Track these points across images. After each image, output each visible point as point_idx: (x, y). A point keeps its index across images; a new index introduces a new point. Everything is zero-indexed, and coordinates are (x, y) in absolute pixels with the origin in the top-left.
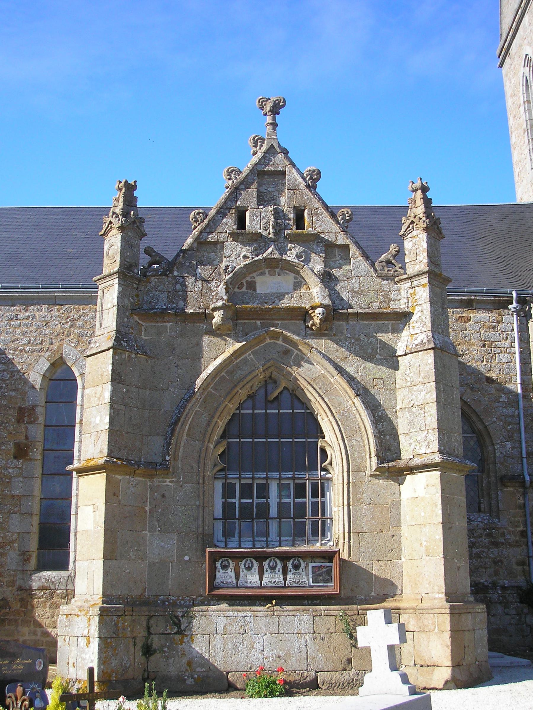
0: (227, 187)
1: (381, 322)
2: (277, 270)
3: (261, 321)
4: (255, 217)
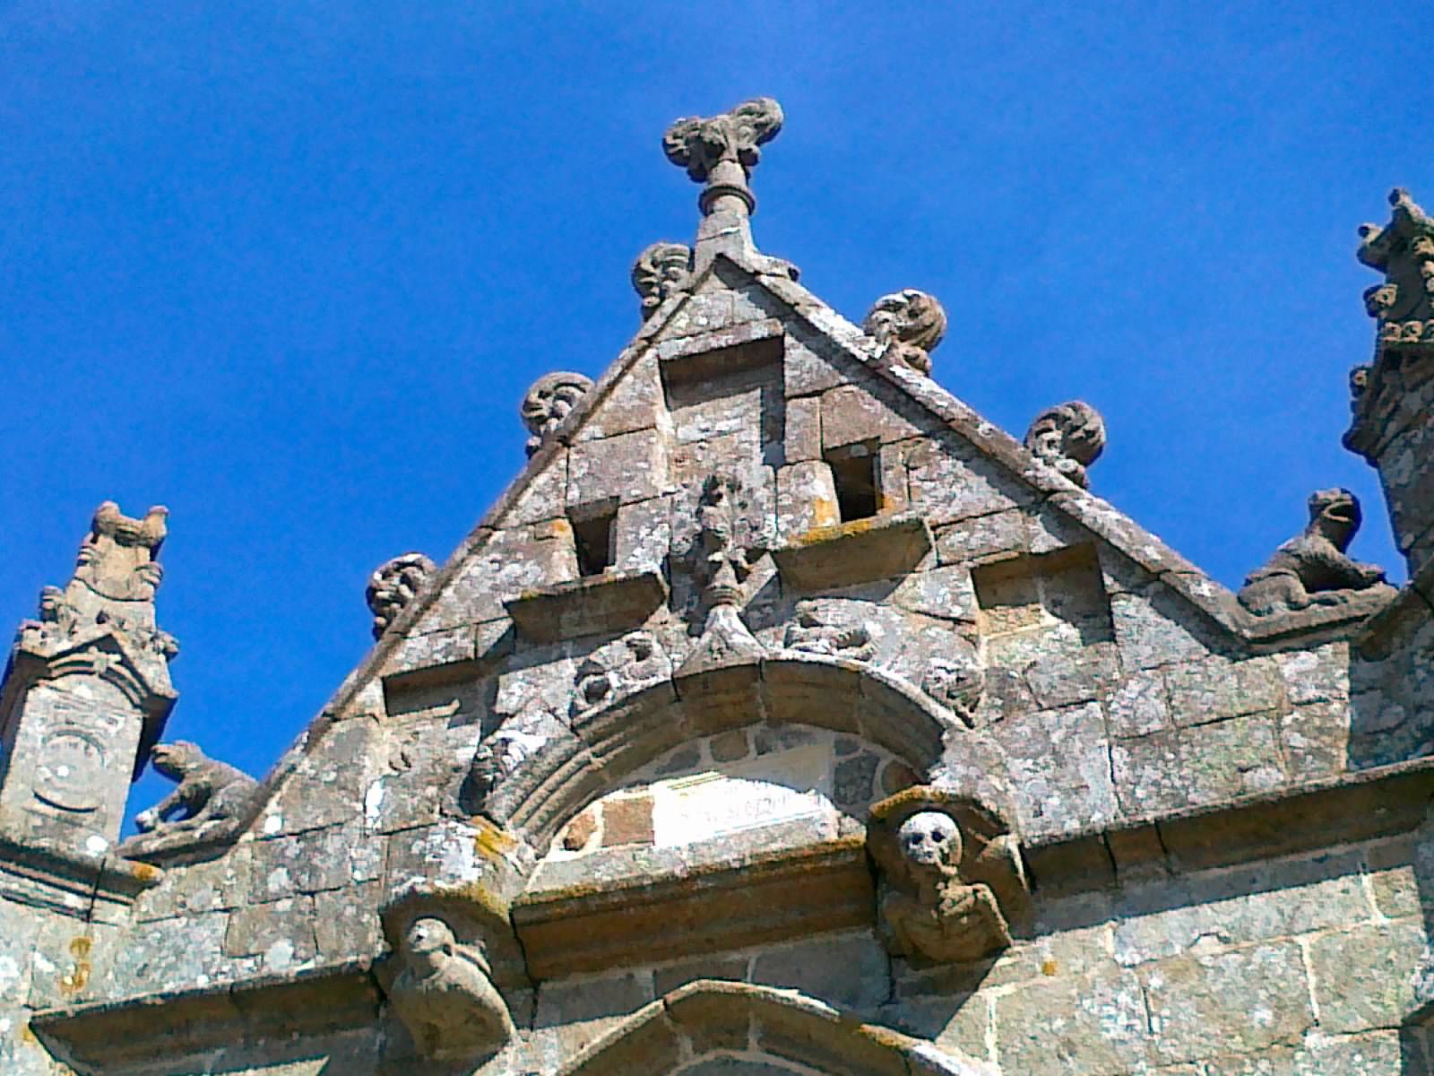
0: (537, 510)
1: (1309, 856)
2: (752, 732)
3: (659, 967)
4: (643, 532)
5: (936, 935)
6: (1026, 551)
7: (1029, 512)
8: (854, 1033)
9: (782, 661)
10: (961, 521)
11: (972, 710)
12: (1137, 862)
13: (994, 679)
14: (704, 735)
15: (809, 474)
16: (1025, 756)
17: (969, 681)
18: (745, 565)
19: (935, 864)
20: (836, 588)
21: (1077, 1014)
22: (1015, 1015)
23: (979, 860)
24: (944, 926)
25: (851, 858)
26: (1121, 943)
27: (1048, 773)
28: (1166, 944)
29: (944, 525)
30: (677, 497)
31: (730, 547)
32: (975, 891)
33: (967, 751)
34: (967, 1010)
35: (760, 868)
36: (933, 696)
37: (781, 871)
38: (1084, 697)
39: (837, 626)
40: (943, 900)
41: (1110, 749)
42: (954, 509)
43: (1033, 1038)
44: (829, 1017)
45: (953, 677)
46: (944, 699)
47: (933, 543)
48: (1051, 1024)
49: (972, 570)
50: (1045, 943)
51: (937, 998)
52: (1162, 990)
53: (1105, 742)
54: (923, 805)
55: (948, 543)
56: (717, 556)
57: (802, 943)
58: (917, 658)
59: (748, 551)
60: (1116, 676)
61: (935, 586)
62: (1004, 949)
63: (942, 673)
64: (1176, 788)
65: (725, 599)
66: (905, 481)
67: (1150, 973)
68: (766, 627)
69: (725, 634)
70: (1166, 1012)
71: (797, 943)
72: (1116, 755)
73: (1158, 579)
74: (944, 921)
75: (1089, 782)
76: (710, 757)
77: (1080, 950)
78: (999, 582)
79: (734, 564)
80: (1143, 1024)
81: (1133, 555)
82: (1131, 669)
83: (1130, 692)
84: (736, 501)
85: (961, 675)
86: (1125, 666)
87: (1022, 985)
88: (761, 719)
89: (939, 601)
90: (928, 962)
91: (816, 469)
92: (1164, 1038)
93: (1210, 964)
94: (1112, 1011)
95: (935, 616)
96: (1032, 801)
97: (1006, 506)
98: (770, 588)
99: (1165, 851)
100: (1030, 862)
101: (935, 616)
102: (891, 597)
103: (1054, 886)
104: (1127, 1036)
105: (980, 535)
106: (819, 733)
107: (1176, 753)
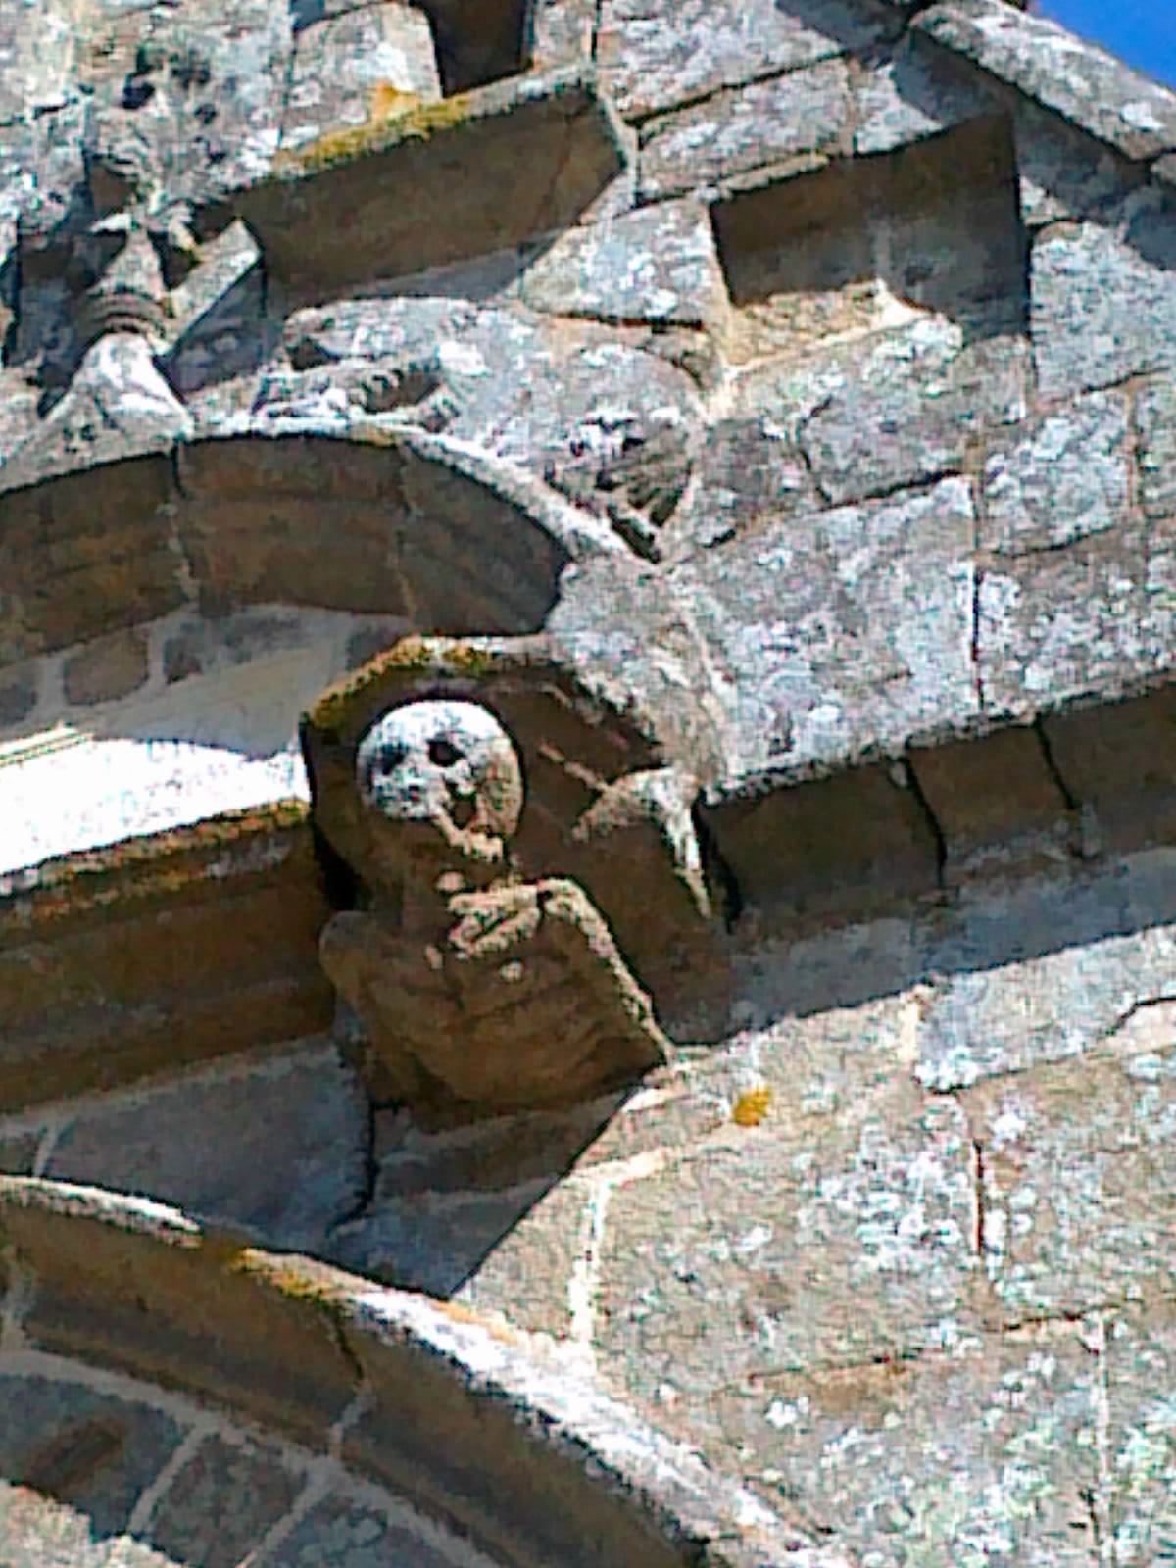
2: (162, 631)
5: (440, 1016)
6: (848, 149)
7: (865, 66)
8: (225, 1270)
9: (223, 439)
10: (706, 98)
11: (657, 520)
12: (1000, 836)
13: (724, 446)
14: (52, 648)
15: (370, 34)
16: (768, 616)
17: (652, 446)
18: (185, 240)
19: (428, 820)
20: (384, 273)
21: (802, 1215)
22: (652, 1227)
23: (580, 833)
24: (455, 988)
25: (276, 854)
26: (937, 1035)
27: (821, 650)
28: (1050, 1030)
29: (662, 111)
30: (62, 117)
31: (154, 205)
32: (543, 897)
33: (610, 599)
34: (538, 1222)
35: (59, 893)
36: (561, 489)
37: (107, 897)
38: (931, 467)
39: (372, 357)
40: (457, 919)
41: (978, 581)
42: (692, 74)
43: (688, 1279)
44: (169, 1237)
45: (617, 439)
46: (588, 491)
47: (631, 153)
48: (732, 1244)
49: (713, 207)
50: (751, 1051)
51: (469, 1198)
52: (1022, 1144)
53: (969, 568)
54: (423, 686)
55: (666, 152)
56: (116, 222)
57: (171, 1088)
58: (552, 418)
59: (197, 209)
60: (1020, 410)
61: (632, 251)
62: (649, 1069)
63: (594, 435)
64: (1125, 659)
65: (126, 321)
66: (587, 25)
67: (998, 1102)
68: (213, 381)
69: (106, 395)
70: (1025, 1197)
71: (158, 1090)
72: (989, 595)
73: (1149, 179)
74: (461, 974)
75: (918, 663)
76: (60, 695)
77: (834, 1061)
78: (777, 234)
79: (159, 241)
80: (964, 1230)
81: (1092, 124)
82: (1057, 391)
83: (1046, 446)
84: (190, 106)
85: (636, 432)
86: (1043, 388)
87: (677, 1154)
88: (186, 599)
89: (626, 282)
90: (466, 1111)
91: (387, 22)
92: (1012, 1259)
93: (1152, 1073)
94: (892, 1202)
95: (612, 321)
96: (772, 716)
97: (815, 53)
98: (239, 294)
99: (1071, 804)
100: (725, 845)
101: (612, 321)
102: (513, 289)
103: (788, 911)
104: (920, 1259)
105: (741, 124)
106: (315, 620)
107: (1138, 577)
